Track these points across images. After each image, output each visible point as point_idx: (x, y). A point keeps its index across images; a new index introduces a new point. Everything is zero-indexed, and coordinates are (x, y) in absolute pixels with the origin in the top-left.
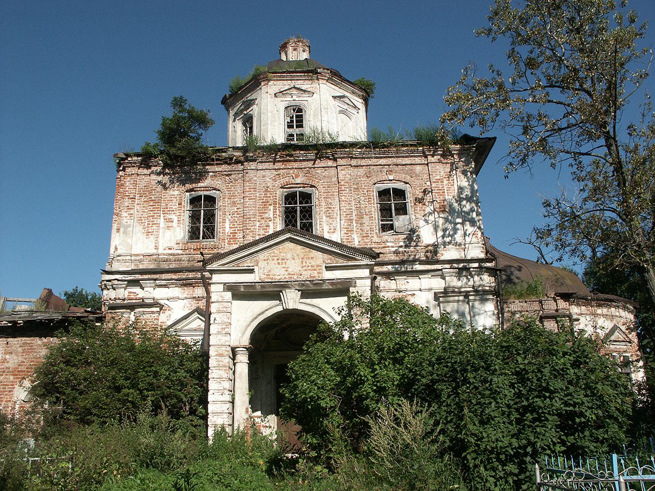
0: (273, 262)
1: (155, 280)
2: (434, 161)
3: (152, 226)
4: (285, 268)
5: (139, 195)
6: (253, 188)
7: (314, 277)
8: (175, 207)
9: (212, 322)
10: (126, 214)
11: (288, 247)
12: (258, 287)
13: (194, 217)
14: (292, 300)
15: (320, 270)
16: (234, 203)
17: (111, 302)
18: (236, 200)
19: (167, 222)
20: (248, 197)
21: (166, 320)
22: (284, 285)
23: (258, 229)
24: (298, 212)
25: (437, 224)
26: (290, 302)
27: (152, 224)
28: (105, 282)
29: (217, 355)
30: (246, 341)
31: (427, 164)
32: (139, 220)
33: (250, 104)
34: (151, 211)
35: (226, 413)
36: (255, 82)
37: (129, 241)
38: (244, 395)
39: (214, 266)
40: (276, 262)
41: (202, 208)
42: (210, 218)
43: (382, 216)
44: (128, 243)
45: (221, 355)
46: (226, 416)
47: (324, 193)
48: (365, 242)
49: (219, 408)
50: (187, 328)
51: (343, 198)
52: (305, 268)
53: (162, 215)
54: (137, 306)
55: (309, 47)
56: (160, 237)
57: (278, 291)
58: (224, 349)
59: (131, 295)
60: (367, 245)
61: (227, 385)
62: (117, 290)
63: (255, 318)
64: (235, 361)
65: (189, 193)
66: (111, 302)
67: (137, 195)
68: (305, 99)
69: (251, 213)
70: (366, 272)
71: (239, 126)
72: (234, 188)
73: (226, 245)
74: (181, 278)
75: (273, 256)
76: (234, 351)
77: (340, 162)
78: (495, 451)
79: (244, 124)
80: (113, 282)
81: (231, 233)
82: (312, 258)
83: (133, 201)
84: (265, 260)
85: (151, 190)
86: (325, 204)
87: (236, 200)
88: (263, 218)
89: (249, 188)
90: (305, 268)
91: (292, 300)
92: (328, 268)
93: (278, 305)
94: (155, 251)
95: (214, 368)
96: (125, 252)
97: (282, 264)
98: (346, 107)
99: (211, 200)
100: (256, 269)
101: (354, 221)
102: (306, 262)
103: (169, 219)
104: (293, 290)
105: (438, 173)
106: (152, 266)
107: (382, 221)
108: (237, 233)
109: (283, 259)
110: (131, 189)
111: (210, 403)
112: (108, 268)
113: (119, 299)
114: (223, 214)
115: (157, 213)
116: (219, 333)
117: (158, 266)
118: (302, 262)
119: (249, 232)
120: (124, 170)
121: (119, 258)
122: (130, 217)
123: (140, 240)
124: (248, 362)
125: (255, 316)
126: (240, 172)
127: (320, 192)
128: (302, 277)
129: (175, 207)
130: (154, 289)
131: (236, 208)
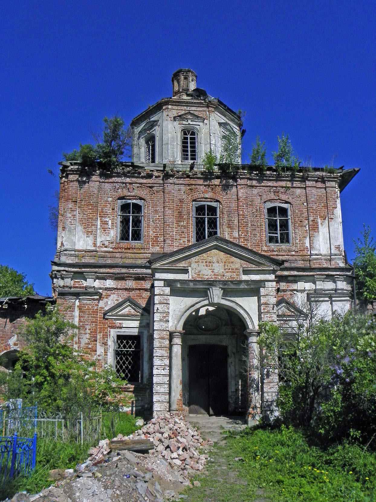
1: (96, 273)
2: (311, 186)
3: (91, 227)
4: (211, 269)
5: (80, 199)
6: (171, 200)
7: (234, 278)
9: (155, 311)
10: (70, 215)
11: (214, 252)
13: (125, 222)
14: (217, 296)
15: (238, 272)
16: (156, 211)
17: (60, 289)
18: (158, 209)
19: (103, 224)
21: (103, 306)
22: (211, 283)
23: (176, 235)
24: (206, 223)
26: (215, 298)
27: (91, 225)
28: (55, 272)
30: (180, 328)
31: (305, 188)
32: (80, 221)
33: (153, 124)
34: (91, 213)
36: (158, 108)
37: (73, 238)
38: (179, 370)
39: (157, 265)
40: (205, 264)
42: (137, 222)
43: (270, 229)
45: (163, 338)
50: (120, 313)
52: (227, 270)
53: (99, 218)
54: (82, 293)
55: (196, 77)
56: (98, 237)
57: (206, 288)
58: (165, 333)
59: (76, 284)
62: (65, 280)
63: (188, 310)
64: (172, 343)
65: (120, 201)
68: (198, 123)
69: (170, 221)
70: (272, 277)
71: (142, 141)
72: (156, 199)
73: (151, 246)
75: (202, 259)
76: (171, 336)
77: (308, 183)
78: (351, 425)
79: (147, 143)
80: (63, 272)
81: (154, 237)
82: (232, 262)
84: (196, 262)
85: (90, 195)
87: (158, 209)
88: (179, 226)
89: (169, 200)
90: (227, 270)
91: (217, 296)
94: (93, 248)
96: (70, 247)
97: (209, 266)
99: (137, 208)
101: (249, 233)
102: (227, 266)
103: (105, 222)
105: (313, 196)
107: (269, 233)
108: (158, 237)
109: (210, 262)
110: (74, 193)
112: (56, 260)
113: (67, 287)
114: (148, 220)
116: (161, 320)
117: (98, 262)
118: (225, 265)
120: (67, 177)
121: (65, 252)
123: (82, 238)
125: (187, 307)
126: (161, 185)
127: (224, 207)
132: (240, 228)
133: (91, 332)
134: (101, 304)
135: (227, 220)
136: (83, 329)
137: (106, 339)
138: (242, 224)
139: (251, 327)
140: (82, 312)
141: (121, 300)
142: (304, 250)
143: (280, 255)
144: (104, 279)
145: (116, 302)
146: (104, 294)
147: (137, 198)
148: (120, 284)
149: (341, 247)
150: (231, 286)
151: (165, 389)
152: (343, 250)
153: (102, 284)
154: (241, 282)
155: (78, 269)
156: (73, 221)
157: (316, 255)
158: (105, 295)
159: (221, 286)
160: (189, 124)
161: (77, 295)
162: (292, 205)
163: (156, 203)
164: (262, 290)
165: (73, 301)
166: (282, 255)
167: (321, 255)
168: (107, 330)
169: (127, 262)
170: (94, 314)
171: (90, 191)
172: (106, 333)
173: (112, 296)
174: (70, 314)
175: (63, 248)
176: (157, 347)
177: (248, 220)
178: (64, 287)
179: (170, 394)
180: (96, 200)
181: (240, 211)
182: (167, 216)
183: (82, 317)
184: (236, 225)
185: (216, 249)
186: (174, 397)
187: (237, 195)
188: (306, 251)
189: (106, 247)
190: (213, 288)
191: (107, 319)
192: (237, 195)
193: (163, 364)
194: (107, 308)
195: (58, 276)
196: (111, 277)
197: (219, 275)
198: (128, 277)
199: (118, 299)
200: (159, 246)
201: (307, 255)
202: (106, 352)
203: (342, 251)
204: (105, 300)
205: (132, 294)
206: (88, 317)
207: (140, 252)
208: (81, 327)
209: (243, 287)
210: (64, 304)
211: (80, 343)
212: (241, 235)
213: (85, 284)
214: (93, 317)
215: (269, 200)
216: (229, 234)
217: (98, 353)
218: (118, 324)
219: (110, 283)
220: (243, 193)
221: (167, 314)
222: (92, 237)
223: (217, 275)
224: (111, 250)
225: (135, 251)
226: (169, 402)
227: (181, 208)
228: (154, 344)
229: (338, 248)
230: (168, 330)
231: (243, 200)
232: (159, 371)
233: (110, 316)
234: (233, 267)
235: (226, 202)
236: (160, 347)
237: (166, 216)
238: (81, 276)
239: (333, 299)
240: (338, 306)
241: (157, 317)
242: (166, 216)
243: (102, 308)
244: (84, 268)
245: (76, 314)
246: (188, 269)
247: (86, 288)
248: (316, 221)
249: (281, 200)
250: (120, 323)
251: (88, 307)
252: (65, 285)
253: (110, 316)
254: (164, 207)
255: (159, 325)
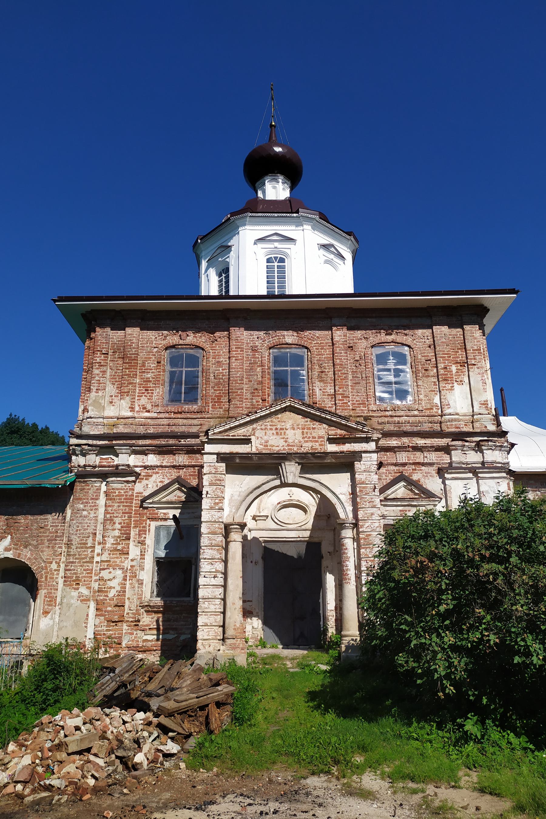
0: (271, 432)
3: (127, 386)
4: (284, 438)
5: (112, 351)
8: (154, 365)
12: (255, 458)
14: (292, 474)
17: (80, 469)
20: (234, 357)
21: (142, 491)
25: (415, 375)
28: (74, 447)
29: (209, 533)
32: (112, 379)
35: (218, 598)
41: (184, 369)
44: (100, 404)
46: (218, 602)
47: (316, 355)
48: (362, 410)
49: (210, 593)
50: (164, 500)
51: (338, 361)
52: (306, 439)
54: (111, 474)
57: (277, 464)
60: (364, 413)
61: (220, 566)
62: (88, 457)
63: (251, 492)
64: (228, 540)
66: (80, 469)
67: (110, 351)
69: (238, 375)
71: (212, 273)
73: (210, 409)
74: (160, 444)
79: (220, 275)
81: (216, 396)
83: (106, 357)
86: (318, 367)
90: (306, 439)
91: (292, 474)
92: (332, 441)
93: (275, 479)
94: (130, 414)
95: (205, 548)
97: (281, 434)
98: (332, 256)
100: (253, 438)
101: (350, 387)
103: (147, 378)
104: (292, 463)
106: (126, 431)
109: (281, 429)
110: (103, 343)
111: (201, 587)
112: (77, 430)
113: (89, 466)
115: (133, 371)
116: (211, 508)
117: (135, 431)
118: (303, 433)
119: (236, 395)
122: (103, 375)
124: (242, 540)
125: (250, 490)
127: (313, 354)
128: (303, 449)
129: (154, 365)
130: (130, 456)
131: (221, 369)
132: (337, 381)
133: (122, 527)
134: (139, 487)
135: (318, 372)
136: (110, 523)
137: (144, 536)
138: (340, 377)
139: (342, 515)
140: (111, 499)
141: (167, 481)
142: (432, 409)
143: (395, 416)
144: (144, 453)
145: (160, 485)
146: (143, 474)
147: (192, 346)
148: (167, 460)
149: (489, 402)
150: (312, 460)
151: (217, 606)
152: (493, 407)
153: (141, 460)
154: (326, 454)
155: (107, 442)
156: (102, 379)
157: (450, 414)
158: (146, 476)
159: (298, 461)
160: (276, 248)
161: (103, 476)
162: (412, 349)
163: (219, 352)
164: (357, 465)
165: (98, 485)
166: (400, 416)
167: (457, 414)
168: (146, 524)
169: (176, 430)
170: (126, 502)
171: (127, 340)
172: (144, 527)
173: (154, 476)
174: (92, 503)
175: (86, 415)
176: (206, 546)
177: (348, 371)
178: (85, 466)
179: (224, 613)
180: (135, 351)
181: (336, 359)
182: (234, 368)
183: (109, 506)
184: (332, 378)
185: (290, 411)
186: (230, 618)
187: (332, 339)
188: (435, 410)
189: (149, 411)
190: (286, 463)
191: (147, 508)
192: (332, 339)
193: (214, 570)
194: (146, 494)
195: (77, 452)
196: (153, 451)
197: (294, 446)
198: (178, 450)
199: (164, 480)
200: (221, 408)
201: (437, 414)
202: (142, 555)
203: (491, 409)
204: (145, 482)
205: (182, 473)
206: (119, 506)
207: (195, 417)
208: (108, 520)
209: (329, 461)
210: (84, 489)
211: (106, 543)
212: (339, 391)
213: (117, 461)
214: (126, 506)
215: (378, 344)
216: (321, 390)
217: (131, 557)
218: (162, 515)
219: (152, 459)
220: (340, 336)
221: (220, 500)
222: (128, 399)
223: (292, 446)
224: (155, 415)
225: (189, 415)
226: (223, 626)
227: (253, 358)
228: (202, 541)
229: (483, 404)
230: (223, 522)
231: (341, 344)
232: (207, 580)
233: (151, 503)
234: (314, 435)
235: (317, 349)
236: (209, 546)
237: (232, 368)
238: (110, 450)
239: (479, 475)
240: (489, 486)
241: (206, 503)
242: (232, 368)
243: (139, 493)
244: (115, 440)
245: (101, 502)
246: (251, 439)
247: (117, 466)
248: (450, 368)
249: (395, 343)
250: (164, 514)
251: (119, 492)
252: (87, 464)
253: (151, 503)
254: (229, 358)
255: (208, 515)
